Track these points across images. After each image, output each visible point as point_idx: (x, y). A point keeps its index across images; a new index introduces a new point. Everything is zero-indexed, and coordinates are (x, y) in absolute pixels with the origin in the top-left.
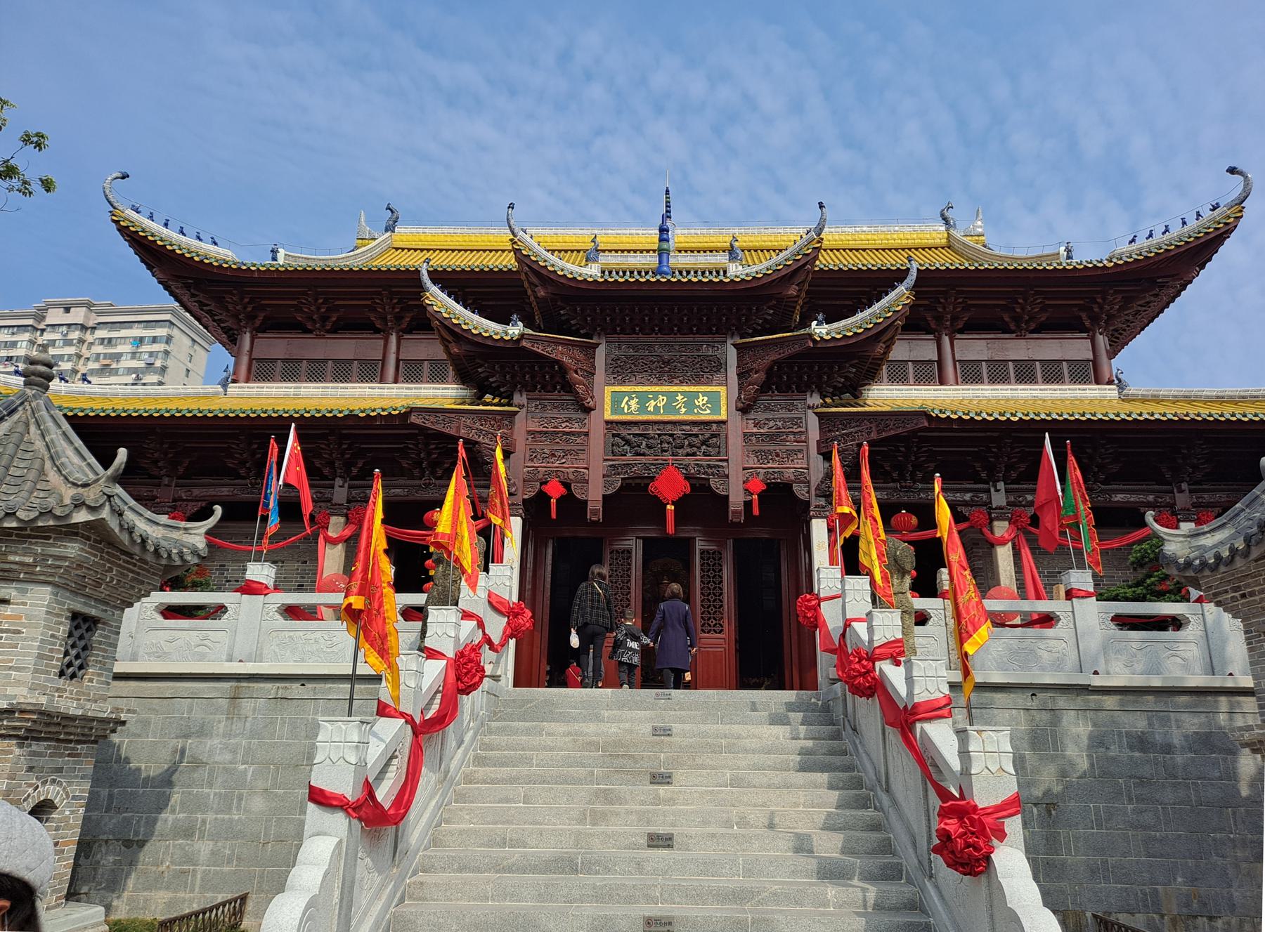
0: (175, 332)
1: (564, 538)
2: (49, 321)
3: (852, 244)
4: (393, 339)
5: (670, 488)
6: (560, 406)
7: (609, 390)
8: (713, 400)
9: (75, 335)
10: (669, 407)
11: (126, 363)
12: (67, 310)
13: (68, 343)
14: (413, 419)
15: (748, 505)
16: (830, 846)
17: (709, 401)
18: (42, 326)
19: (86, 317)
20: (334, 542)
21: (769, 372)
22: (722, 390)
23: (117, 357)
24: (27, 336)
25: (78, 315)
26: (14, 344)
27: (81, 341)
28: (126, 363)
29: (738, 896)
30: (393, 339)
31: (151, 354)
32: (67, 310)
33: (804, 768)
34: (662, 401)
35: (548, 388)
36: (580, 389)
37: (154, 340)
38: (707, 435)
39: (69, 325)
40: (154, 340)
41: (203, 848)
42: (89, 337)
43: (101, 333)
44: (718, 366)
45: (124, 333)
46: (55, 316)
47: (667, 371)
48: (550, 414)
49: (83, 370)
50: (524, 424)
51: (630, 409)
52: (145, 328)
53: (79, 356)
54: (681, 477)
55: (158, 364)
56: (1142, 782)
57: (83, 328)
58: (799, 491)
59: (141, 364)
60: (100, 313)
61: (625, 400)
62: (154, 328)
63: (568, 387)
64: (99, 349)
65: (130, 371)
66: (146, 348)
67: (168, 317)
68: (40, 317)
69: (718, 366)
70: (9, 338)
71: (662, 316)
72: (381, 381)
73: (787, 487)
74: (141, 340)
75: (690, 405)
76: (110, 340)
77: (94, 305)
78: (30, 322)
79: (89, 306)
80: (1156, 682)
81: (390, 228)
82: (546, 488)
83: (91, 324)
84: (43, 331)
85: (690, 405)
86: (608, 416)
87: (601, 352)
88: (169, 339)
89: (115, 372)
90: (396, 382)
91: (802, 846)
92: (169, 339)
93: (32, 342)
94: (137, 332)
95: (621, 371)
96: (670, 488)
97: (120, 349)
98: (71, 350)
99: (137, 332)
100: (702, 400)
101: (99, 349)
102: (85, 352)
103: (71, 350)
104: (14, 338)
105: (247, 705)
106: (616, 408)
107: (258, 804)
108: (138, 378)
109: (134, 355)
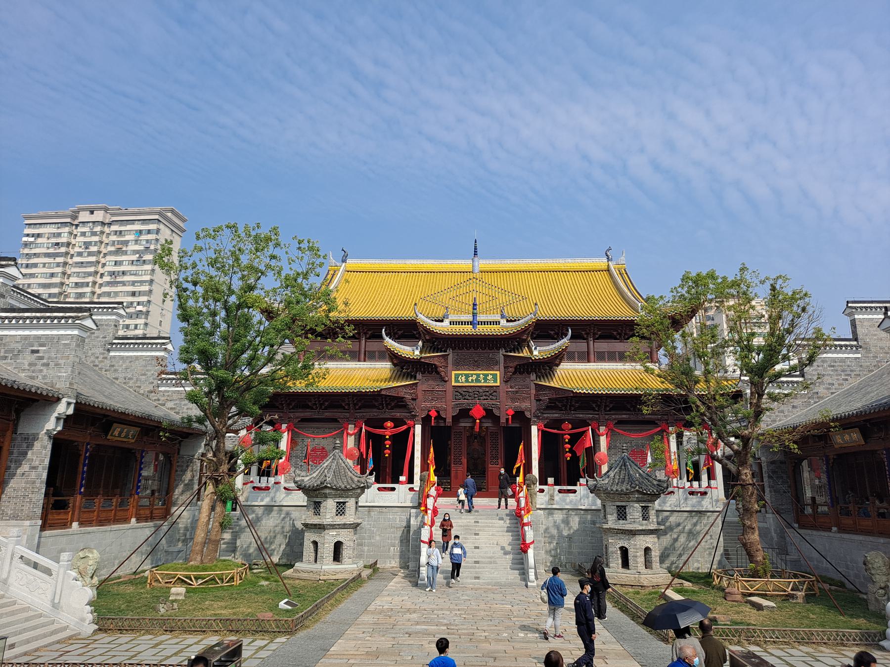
0: (162, 227)
1: (439, 436)
2: (81, 219)
3: (563, 268)
4: (363, 342)
5: (478, 412)
6: (434, 380)
7: (453, 372)
8: (494, 376)
9: (98, 229)
10: (477, 380)
11: (132, 247)
12: (92, 212)
13: (94, 234)
14: (383, 393)
15: (507, 420)
16: (509, 548)
17: (492, 378)
18: (76, 222)
19: (104, 217)
20: (351, 435)
21: (516, 368)
22: (498, 373)
23: (126, 243)
24: (67, 229)
25: (99, 216)
26: (59, 235)
27: (102, 232)
28: (132, 247)
29: (490, 558)
30: (363, 342)
31: (147, 241)
32: (92, 212)
33: (507, 531)
34: (474, 377)
35: (430, 373)
36: (443, 374)
37: (149, 232)
38: (492, 391)
39: (94, 222)
40: (149, 232)
41: (366, 548)
42: (106, 230)
43: (115, 228)
44: (497, 363)
45: (129, 227)
46: (84, 216)
47: (476, 365)
48: (431, 382)
49: (104, 251)
50: (422, 387)
51: (462, 382)
52: (142, 224)
53: (101, 242)
54: (481, 408)
55: (152, 247)
56: (593, 532)
57: (103, 224)
58: (528, 414)
59: (142, 248)
60: (113, 215)
61: (461, 377)
62: (148, 224)
63: (438, 373)
64: (113, 238)
65: (135, 252)
66: (144, 237)
67: (157, 217)
68: (75, 217)
69: (497, 363)
70: (55, 231)
71: (475, 347)
72: (359, 361)
73: (523, 412)
74: (141, 232)
75: (485, 379)
76: (121, 232)
77: (108, 209)
78: (68, 220)
79: (106, 210)
80: (593, 508)
81: (344, 261)
82: (431, 413)
83: (107, 221)
84: (77, 226)
85: (485, 379)
86: (453, 384)
87: (450, 358)
88: (158, 231)
89: (125, 253)
90: (365, 361)
91: (503, 548)
92: (158, 231)
93: (71, 233)
94: (137, 227)
95: (458, 365)
96: (478, 412)
97: (127, 238)
98: (96, 239)
99: (137, 227)
100: (490, 377)
101: (113, 238)
102: (106, 240)
103: (96, 239)
104: (59, 231)
105: (372, 514)
106: (457, 381)
107: (378, 538)
108: (140, 257)
109: (136, 242)
